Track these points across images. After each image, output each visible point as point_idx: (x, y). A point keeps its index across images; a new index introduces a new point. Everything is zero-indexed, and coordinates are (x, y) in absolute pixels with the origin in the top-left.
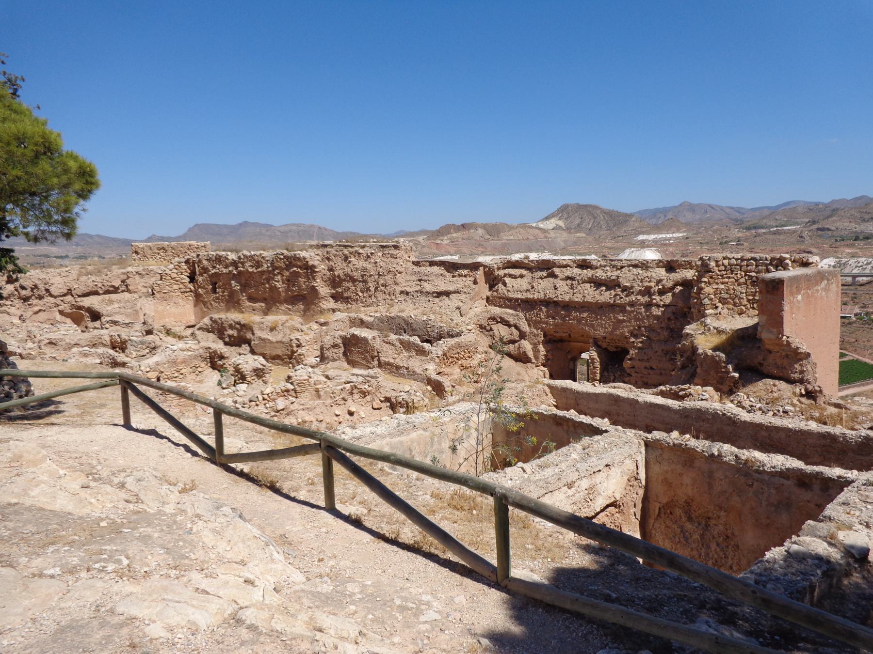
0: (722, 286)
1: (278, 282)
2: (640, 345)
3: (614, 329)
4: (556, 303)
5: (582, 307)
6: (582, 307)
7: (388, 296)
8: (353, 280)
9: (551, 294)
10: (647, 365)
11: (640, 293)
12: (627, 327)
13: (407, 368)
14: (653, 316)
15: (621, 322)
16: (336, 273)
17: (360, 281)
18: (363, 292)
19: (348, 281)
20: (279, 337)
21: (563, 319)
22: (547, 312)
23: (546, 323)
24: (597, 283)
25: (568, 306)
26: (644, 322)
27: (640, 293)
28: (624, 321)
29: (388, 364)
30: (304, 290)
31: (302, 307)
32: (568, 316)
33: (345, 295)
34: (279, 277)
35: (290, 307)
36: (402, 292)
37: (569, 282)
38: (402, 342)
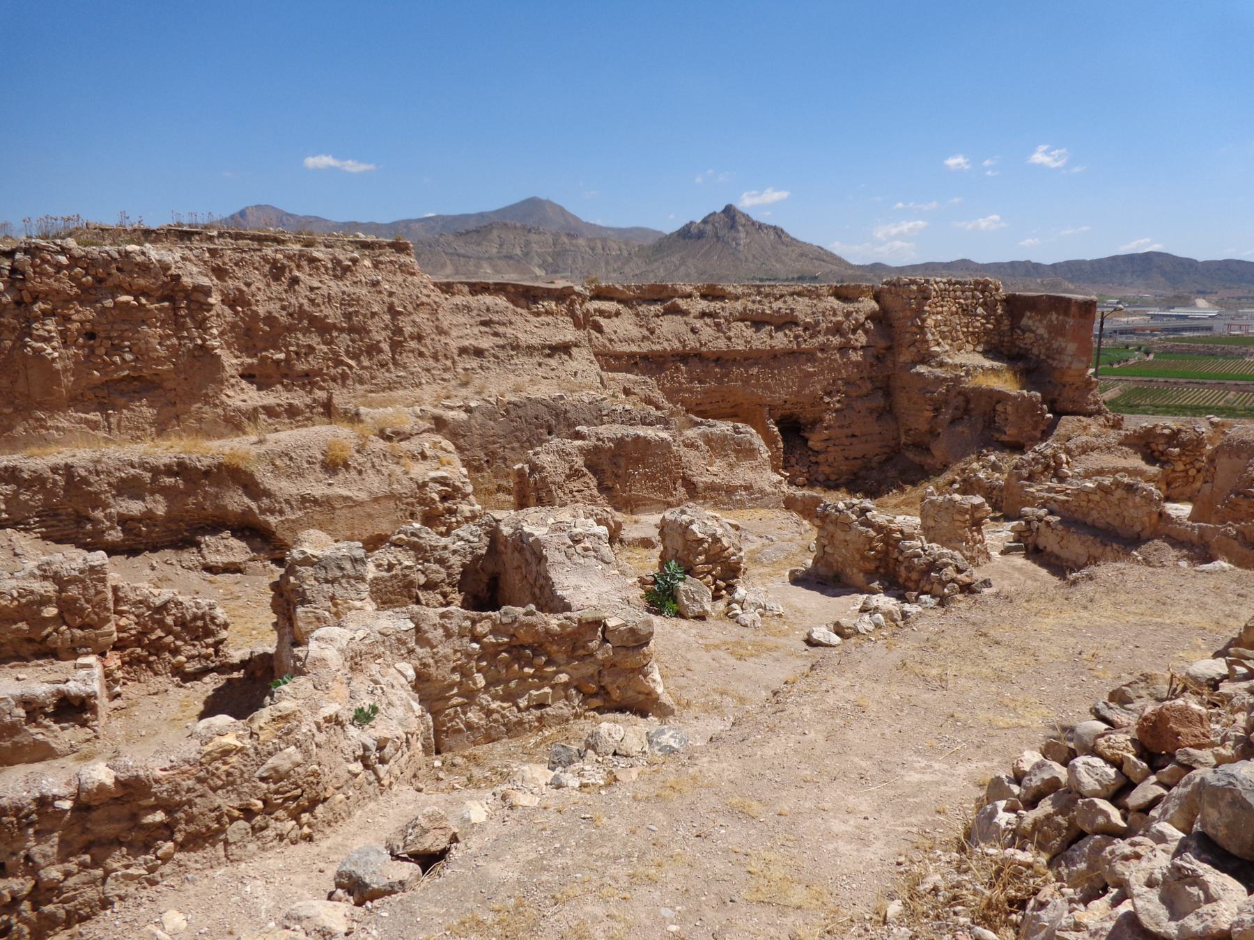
0: (939, 317)
1: (47, 340)
2: (838, 406)
3: (801, 388)
4: (699, 356)
5: (746, 359)
6: (746, 359)
7: (431, 362)
8: (322, 327)
9: (692, 342)
10: (849, 431)
11: (828, 331)
12: (819, 381)
13: (746, 488)
14: (852, 363)
15: (811, 375)
16: (261, 311)
17: (341, 330)
18: (355, 357)
19: (306, 331)
20: (375, 483)
21: (719, 381)
22: (690, 372)
23: (690, 391)
24: (758, 323)
25: (720, 359)
26: (840, 373)
27: (828, 331)
28: (814, 374)
29: (712, 487)
30: (158, 361)
31: (148, 412)
32: (727, 375)
33: (302, 366)
34: (51, 325)
35: (94, 416)
36: (463, 351)
37: (708, 320)
38: (708, 440)
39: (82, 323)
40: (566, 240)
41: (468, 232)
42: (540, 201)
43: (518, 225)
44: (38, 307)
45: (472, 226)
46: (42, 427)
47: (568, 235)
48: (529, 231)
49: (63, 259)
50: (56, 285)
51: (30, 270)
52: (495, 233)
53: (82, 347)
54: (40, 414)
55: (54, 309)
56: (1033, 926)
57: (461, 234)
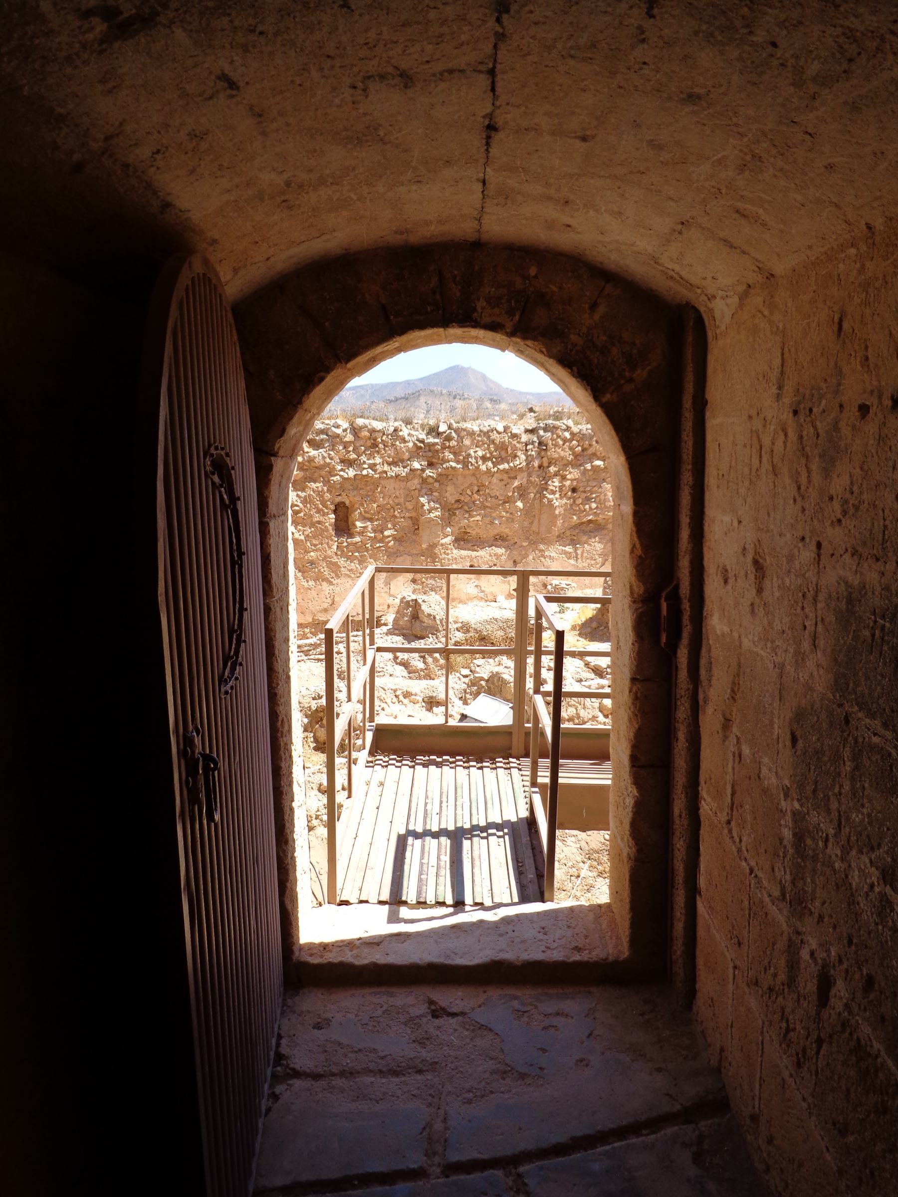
35: (569, 549)
39: (572, 480)
40: (489, 406)
41: (397, 399)
42: (463, 368)
43: (444, 392)
44: (552, 469)
45: (400, 393)
46: (543, 556)
47: (491, 400)
48: (455, 398)
49: (567, 435)
50: (562, 454)
51: (550, 442)
52: (422, 399)
53: (569, 499)
54: (542, 547)
55: (559, 471)
56: (528, 1193)
57: (391, 401)
